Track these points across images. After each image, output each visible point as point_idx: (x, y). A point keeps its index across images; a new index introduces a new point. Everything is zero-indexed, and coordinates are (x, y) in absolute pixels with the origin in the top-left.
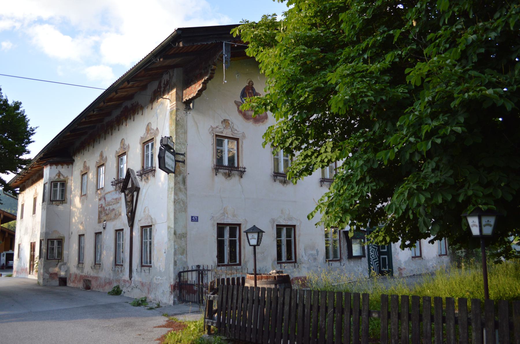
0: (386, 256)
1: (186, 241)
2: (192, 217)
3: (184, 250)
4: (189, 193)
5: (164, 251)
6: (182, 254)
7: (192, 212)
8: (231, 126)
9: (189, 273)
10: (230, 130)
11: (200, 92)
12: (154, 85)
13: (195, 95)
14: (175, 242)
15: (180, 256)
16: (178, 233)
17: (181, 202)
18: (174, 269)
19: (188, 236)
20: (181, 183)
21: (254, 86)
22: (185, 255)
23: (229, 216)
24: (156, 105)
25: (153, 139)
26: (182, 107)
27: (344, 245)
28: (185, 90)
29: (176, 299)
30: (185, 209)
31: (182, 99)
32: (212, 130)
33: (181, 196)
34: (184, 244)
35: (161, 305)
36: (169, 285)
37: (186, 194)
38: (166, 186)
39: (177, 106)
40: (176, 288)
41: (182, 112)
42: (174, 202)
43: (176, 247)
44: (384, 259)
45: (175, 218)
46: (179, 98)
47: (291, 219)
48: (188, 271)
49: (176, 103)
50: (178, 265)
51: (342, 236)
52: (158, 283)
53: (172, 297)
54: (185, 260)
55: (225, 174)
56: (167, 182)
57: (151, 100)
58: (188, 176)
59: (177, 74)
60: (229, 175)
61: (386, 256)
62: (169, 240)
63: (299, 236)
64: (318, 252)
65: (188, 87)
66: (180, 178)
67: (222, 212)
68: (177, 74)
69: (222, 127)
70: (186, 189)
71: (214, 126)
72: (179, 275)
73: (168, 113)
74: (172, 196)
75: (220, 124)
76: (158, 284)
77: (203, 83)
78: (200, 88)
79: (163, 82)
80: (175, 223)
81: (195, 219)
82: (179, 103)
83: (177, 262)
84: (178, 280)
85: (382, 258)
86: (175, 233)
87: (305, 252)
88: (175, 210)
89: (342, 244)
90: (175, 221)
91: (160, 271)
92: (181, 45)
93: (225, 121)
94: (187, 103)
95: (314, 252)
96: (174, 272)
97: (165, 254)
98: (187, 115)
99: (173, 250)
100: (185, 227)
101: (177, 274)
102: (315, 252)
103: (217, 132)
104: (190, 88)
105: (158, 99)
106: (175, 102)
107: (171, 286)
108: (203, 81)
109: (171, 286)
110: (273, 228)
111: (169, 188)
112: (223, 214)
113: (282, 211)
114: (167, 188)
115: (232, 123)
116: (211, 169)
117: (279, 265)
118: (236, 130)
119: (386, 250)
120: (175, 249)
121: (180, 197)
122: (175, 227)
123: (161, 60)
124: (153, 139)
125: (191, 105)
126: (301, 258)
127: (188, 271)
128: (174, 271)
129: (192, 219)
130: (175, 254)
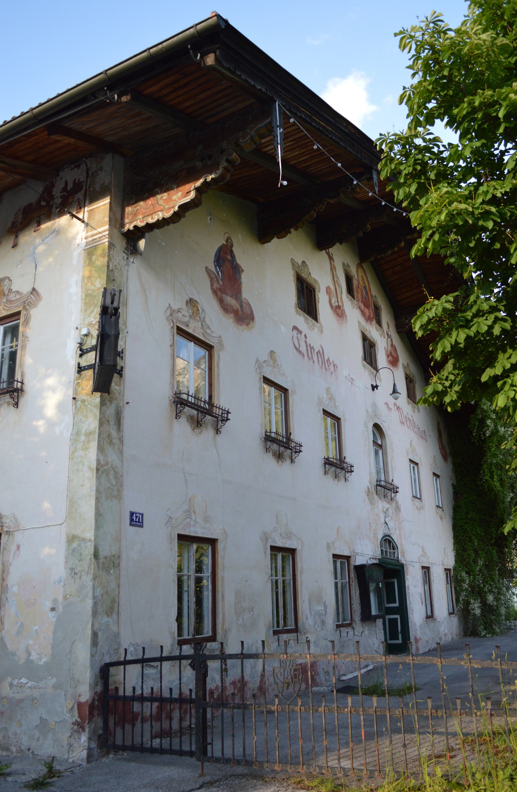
0: (398, 617)
1: (118, 578)
2: (132, 514)
3: (113, 601)
4: (127, 450)
5: (49, 605)
6: (109, 612)
7: (133, 502)
8: (202, 317)
9: (166, 665)
10: (200, 324)
11: (184, 208)
12: (31, 194)
13: (168, 215)
14: (95, 578)
15: (105, 619)
16: (102, 553)
17: (112, 472)
18: (92, 656)
19: (123, 564)
20: (112, 422)
21: (234, 249)
22: (115, 616)
23: (199, 520)
24: (27, 238)
25: (18, 313)
26: (121, 244)
27: (356, 592)
28: (129, 205)
29: (94, 745)
30: (118, 491)
31: (122, 225)
32: (171, 315)
33: (112, 457)
34: (113, 585)
35: (57, 767)
36: (70, 703)
37: (121, 452)
38: (65, 430)
39: (110, 235)
40: (96, 713)
41: (120, 254)
42: (98, 470)
43: (98, 592)
44: (393, 622)
45: (98, 514)
46: (116, 220)
47: (289, 535)
48: (126, 663)
49: (110, 230)
50: (100, 644)
51: (352, 575)
52: (19, 696)
53: (84, 738)
54: (114, 628)
55: (191, 419)
56: (68, 419)
57: (14, 224)
58: (127, 407)
59: (109, 169)
60: (197, 424)
61: (398, 617)
62: (73, 572)
63: (301, 573)
64: (325, 606)
65: (144, 199)
66: (111, 410)
67: (186, 507)
68: (109, 169)
69: (187, 314)
70: (121, 440)
71: (175, 307)
72: (104, 672)
73: (77, 254)
74: (92, 455)
75: (184, 307)
76: (22, 701)
77: (197, 189)
78: (188, 199)
79: (59, 185)
80: (98, 526)
81: (136, 520)
82: (116, 231)
83: (100, 634)
84: (99, 689)
85: (389, 619)
86: (96, 555)
87: (310, 609)
88: (98, 491)
89: (353, 592)
90: (96, 520)
91: (29, 662)
92: (210, 60)
93: (191, 302)
94: (132, 237)
95: (321, 608)
96: (92, 666)
97: (51, 614)
98: (127, 265)
99: (90, 603)
100: (118, 539)
101: (98, 670)
102: (323, 608)
103: (180, 322)
104: (150, 201)
105: (39, 224)
106: (107, 227)
107: (80, 705)
108: (198, 183)
109: (80, 705)
110: (265, 553)
111: (76, 434)
112: (189, 512)
113: (277, 516)
114: (67, 435)
115: (203, 310)
116: (168, 400)
117: (276, 637)
118: (210, 328)
119: (397, 605)
120: (94, 597)
121: (110, 459)
122: (96, 536)
123: (124, 99)
124: (18, 313)
125: (142, 244)
126: (305, 620)
127: (126, 663)
128: (91, 662)
129: (132, 520)
130: (95, 614)
